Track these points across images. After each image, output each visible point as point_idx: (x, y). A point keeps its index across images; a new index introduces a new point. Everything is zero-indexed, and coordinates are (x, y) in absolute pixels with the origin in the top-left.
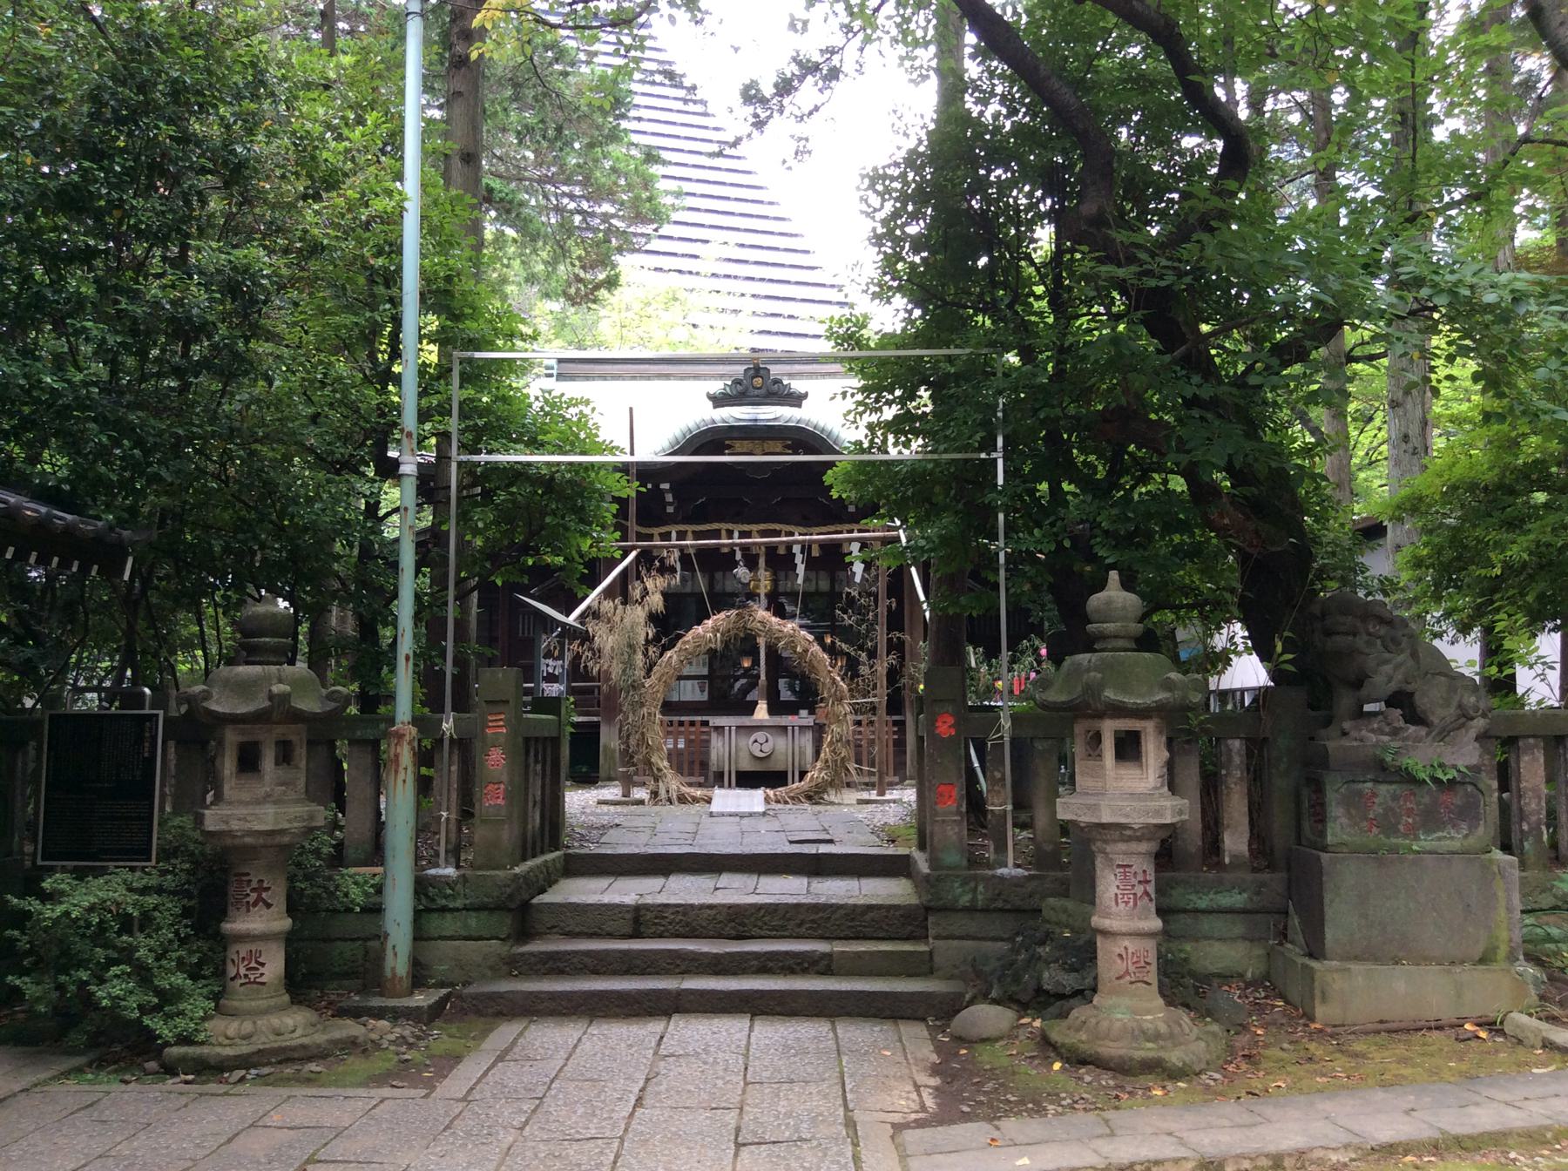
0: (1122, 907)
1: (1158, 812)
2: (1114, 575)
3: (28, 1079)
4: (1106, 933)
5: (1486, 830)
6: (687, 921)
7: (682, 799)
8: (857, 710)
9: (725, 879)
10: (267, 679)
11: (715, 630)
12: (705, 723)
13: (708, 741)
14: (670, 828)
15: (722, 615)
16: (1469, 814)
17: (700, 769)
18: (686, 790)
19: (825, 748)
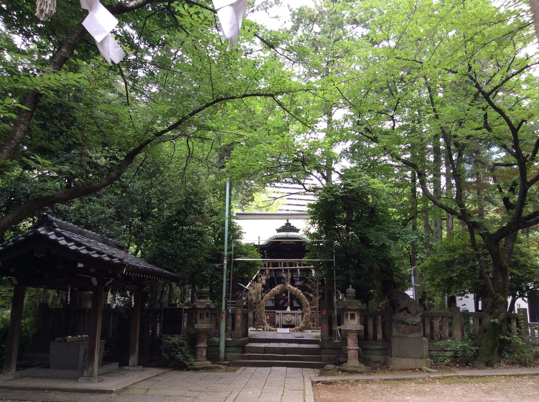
0: (352, 345)
1: (357, 328)
2: (351, 286)
3: (166, 370)
4: (349, 350)
5: (422, 334)
6: (275, 350)
7: (270, 330)
8: (312, 309)
9: (281, 344)
10: (205, 302)
11: (278, 289)
12: (274, 312)
13: (275, 317)
14: (270, 335)
15: (279, 286)
16: (419, 330)
17: (274, 324)
18: (271, 328)
19: (304, 319)
